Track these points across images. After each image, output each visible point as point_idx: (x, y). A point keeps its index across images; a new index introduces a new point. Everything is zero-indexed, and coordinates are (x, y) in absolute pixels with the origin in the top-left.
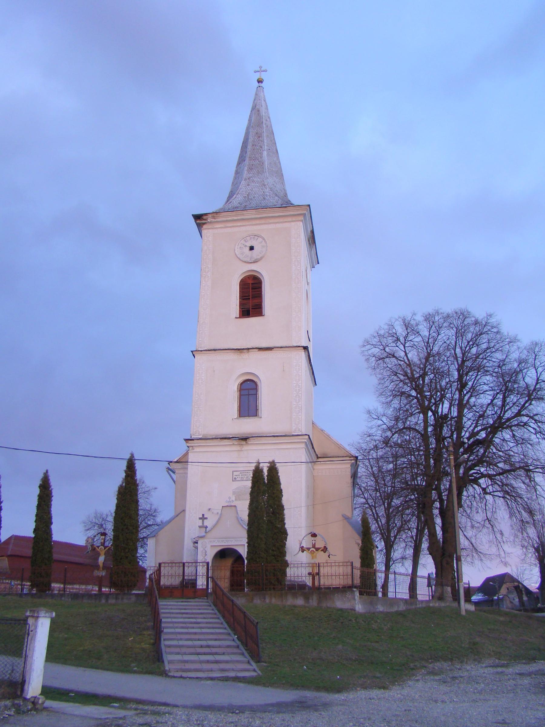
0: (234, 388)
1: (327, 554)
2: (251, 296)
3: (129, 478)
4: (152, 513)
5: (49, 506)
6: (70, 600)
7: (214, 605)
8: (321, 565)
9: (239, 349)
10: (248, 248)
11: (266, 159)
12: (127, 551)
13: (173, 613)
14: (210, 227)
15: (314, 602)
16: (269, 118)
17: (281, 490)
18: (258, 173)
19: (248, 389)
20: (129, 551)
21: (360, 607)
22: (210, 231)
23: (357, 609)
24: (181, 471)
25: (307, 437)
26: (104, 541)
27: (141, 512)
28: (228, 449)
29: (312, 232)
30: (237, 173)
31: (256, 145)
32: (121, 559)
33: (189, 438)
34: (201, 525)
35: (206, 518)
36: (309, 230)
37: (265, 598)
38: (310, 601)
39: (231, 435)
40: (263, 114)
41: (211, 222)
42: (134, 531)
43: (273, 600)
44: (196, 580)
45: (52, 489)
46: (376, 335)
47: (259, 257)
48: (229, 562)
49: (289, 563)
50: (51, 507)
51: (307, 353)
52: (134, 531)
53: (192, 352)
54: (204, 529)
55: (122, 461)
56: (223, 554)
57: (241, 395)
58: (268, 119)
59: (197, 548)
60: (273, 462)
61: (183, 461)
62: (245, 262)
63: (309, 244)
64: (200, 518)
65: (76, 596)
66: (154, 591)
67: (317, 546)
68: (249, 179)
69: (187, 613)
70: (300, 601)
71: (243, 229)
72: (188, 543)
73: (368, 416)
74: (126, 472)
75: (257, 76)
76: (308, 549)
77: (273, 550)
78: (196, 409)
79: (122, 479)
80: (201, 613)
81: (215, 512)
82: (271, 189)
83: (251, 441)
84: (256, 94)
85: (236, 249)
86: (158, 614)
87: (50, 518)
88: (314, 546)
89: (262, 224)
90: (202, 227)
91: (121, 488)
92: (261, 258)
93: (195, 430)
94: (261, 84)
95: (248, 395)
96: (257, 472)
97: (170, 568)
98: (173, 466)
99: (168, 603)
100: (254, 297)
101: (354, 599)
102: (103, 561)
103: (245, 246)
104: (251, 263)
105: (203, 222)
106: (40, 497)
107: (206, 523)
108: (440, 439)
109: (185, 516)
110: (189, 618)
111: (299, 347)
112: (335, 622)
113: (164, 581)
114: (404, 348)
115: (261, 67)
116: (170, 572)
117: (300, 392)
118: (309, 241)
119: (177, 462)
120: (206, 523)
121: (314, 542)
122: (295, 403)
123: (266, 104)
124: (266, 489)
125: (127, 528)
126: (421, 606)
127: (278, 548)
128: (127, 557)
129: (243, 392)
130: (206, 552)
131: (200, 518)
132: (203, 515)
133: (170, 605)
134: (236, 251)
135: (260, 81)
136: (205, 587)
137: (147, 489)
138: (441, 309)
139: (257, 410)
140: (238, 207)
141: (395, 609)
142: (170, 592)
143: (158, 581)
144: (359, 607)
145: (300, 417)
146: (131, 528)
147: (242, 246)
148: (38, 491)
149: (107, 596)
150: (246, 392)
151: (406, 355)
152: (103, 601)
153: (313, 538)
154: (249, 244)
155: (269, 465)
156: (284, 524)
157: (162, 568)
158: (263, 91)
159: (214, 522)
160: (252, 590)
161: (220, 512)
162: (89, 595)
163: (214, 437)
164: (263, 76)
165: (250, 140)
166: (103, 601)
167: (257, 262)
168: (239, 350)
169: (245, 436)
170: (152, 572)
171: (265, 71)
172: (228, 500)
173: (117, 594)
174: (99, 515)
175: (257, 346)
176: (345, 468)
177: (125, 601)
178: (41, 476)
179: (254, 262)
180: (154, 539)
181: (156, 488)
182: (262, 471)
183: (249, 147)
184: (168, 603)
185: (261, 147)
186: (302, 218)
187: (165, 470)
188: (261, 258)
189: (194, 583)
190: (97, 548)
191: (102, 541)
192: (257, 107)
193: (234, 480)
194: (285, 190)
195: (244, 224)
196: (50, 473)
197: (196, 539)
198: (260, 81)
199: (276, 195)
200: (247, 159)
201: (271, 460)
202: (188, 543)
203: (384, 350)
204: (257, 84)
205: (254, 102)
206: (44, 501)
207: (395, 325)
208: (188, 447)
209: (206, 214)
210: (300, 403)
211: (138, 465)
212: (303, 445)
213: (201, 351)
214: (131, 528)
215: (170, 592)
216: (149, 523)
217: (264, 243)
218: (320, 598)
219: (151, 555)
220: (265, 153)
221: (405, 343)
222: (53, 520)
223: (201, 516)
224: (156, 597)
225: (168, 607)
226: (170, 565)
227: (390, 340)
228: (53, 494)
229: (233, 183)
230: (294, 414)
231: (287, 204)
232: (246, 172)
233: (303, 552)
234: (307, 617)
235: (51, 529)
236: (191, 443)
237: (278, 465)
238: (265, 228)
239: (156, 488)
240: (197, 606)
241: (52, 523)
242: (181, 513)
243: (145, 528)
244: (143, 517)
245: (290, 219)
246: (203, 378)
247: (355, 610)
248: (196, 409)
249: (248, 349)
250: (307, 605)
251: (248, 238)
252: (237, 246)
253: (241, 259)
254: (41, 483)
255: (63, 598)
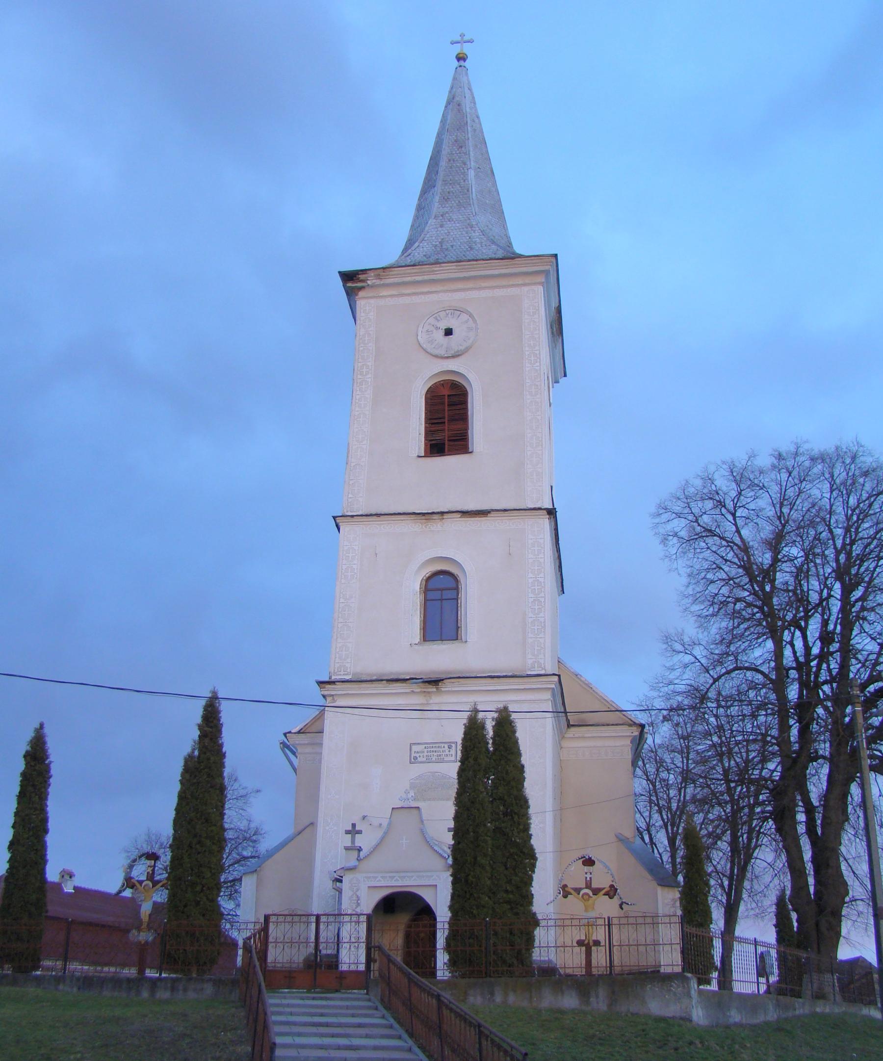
0: (414, 585)
1: (616, 901)
2: (447, 421)
3: (207, 741)
4: (251, 837)
5: (43, 797)
6: (75, 990)
7: (385, 1008)
8: (615, 921)
9: (424, 514)
10: (442, 333)
11: (474, 183)
12: (198, 888)
13: (295, 1024)
14: (371, 294)
15: (600, 1002)
16: (478, 117)
17: (523, 766)
18: (460, 205)
19: (442, 590)
20: (202, 891)
21: (700, 1013)
22: (372, 301)
23: (695, 1018)
24: (308, 750)
25: (556, 679)
26: (153, 871)
27: (229, 835)
28: (400, 701)
29: (559, 310)
30: (419, 208)
31: (456, 164)
32: (185, 906)
33: (327, 679)
34: (349, 844)
35: (360, 832)
36: (554, 304)
37: (492, 994)
38: (593, 999)
39: (408, 674)
40: (468, 110)
41: (372, 287)
42: (215, 848)
43: (511, 998)
44: (337, 956)
45: (51, 762)
46: (679, 494)
47: (462, 348)
48: (402, 920)
49: (539, 917)
50: (46, 799)
51: (553, 523)
52: (215, 848)
53: (334, 518)
54: (355, 853)
55: (194, 700)
56: (392, 904)
57: (426, 600)
58: (477, 121)
59: (340, 891)
60: (506, 709)
61: (313, 729)
62: (436, 356)
63: (552, 333)
64: (347, 832)
65: (87, 982)
66: (255, 973)
67: (594, 885)
68: (442, 216)
69: (327, 1025)
70: (570, 1001)
71: (435, 297)
72: (321, 883)
73: (665, 646)
74: (200, 727)
75: (457, 49)
76: (577, 890)
77: (507, 891)
78: (340, 625)
79: (191, 743)
80: (360, 1026)
81: (376, 822)
82: (483, 232)
83: (446, 686)
84: (455, 79)
85: (420, 334)
86: (266, 1027)
87: (45, 820)
88: (588, 885)
89: (468, 289)
90: (357, 295)
91: (189, 759)
92: (467, 350)
93: (337, 665)
94: (462, 63)
95: (442, 602)
96: (473, 729)
97: (288, 926)
98: (293, 740)
99: (285, 1001)
100: (452, 420)
101: (689, 996)
102: (148, 912)
103: (437, 328)
104: (447, 358)
105: (359, 285)
106: (26, 778)
107: (360, 841)
108: (809, 685)
109: (312, 844)
110: (333, 1036)
111: (540, 509)
112: (660, 1048)
113: (276, 955)
114: (734, 519)
115: (462, 35)
116: (288, 935)
117: (542, 595)
118: (552, 327)
119: (299, 732)
120: (360, 841)
121: (588, 876)
122: (531, 615)
123: (472, 94)
124: (489, 766)
125: (199, 842)
126: (801, 1011)
127: (518, 888)
128: (198, 903)
129: (431, 595)
130: (358, 898)
131: (347, 832)
132: (354, 825)
133: (288, 1005)
134: (419, 338)
135: (461, 58)
136: (362, 967)
137: (242, 792)
138: (807, 442)
139: (458, 628)
140: (426, 260)
141: (760, 1019)
142: (286, 979)
143: (263, 955)
144: (699, 1015)
145: (542, 640)
146: (208, 843)
147: (432, 328)
148: (21, 765)
149: (154, 983)
150: (437, 595)
151: (738, 531)
152: (145, 994)
153: (586, 869)
154: (444, 325)
155: (495, 715)
156: (530, 836)
157: (272, 927)
158: (467, 74)
159: (374, 843)
160: (463, 976)
161: (385, 823)
162: (116, 982)
163: (375, 678)
164: (467, 49)
165: (443, 152)
166: (145, 994)
167: (459, 355)
168: (426, 516)
169: (434, 677)
170: (249, 934)
171: (471, 41)
172: (404, 796)
173: (174, 980)
174: (154, 837)
175: (459, 509)
176: (619, 744)
177: (191, 995)
178: (30, 734)
179: (453, 357)
180: (255, 876)
181: (258, 791)
182: (483, 727)
183: (443, 163)
184: (285, 1001)
185: (465, 164)
186: (541, 278)
187: (278, 747)
188: (467, 350)
189: (333, 962)
190: (138, 885)
191: (150, 870)
192: (457, 99)
193: (414, 760)
194: (508, 238)
195: (434, 289)
196: (47, 730)
197: (339, 873)
198: (461, 58)
199: (493, 242)
200: (439, 184)
201: (501, 706)
202: (321, 883)
203: (697, 521)
204: (456, 63)
205: (450, 92)
206: (33, 785)
207: (716, 476)
208: (324, 696)
209: (364, 271)
210: (542, 615)
211: (227, 713)
212: (548, 695)
213: (352, 516)
214: (208, 843)
215: (286, 979)
216: (245, 853)
217: (471, 323)
218: (613, 992)
219: (245, 907)
220: (471, 174)
221: (735, 511)
222: (51, 825)
223: (350, 828)
224: (260, 986)
225: (286, 1010)
226: (289, 919)
227: (709, 504)
228: (52, 772)
229: (412, 226)
230: (530, 635)
231: (512, 256)
232: (436, 204)
233: (565, 896)
234: (594, 1036)
235: (45, 842)
236: (329, 690)
237: (513, 716)
238: (476, 297)
239: (258, 791)
240: (347, 1007)
241: (46, 831)
242: (306, 829)
243: (238, 862)
244: (233, 842)
245: (519, 281)
246: (355, 567)
247: (691, 1021)
248: (340, 625)
249: (442, 513)
250: (584, 1007)
251: (442, 314)
252: (420, 329)
253: (429, 350)
254: (29, 748)
255: (61, 987)
